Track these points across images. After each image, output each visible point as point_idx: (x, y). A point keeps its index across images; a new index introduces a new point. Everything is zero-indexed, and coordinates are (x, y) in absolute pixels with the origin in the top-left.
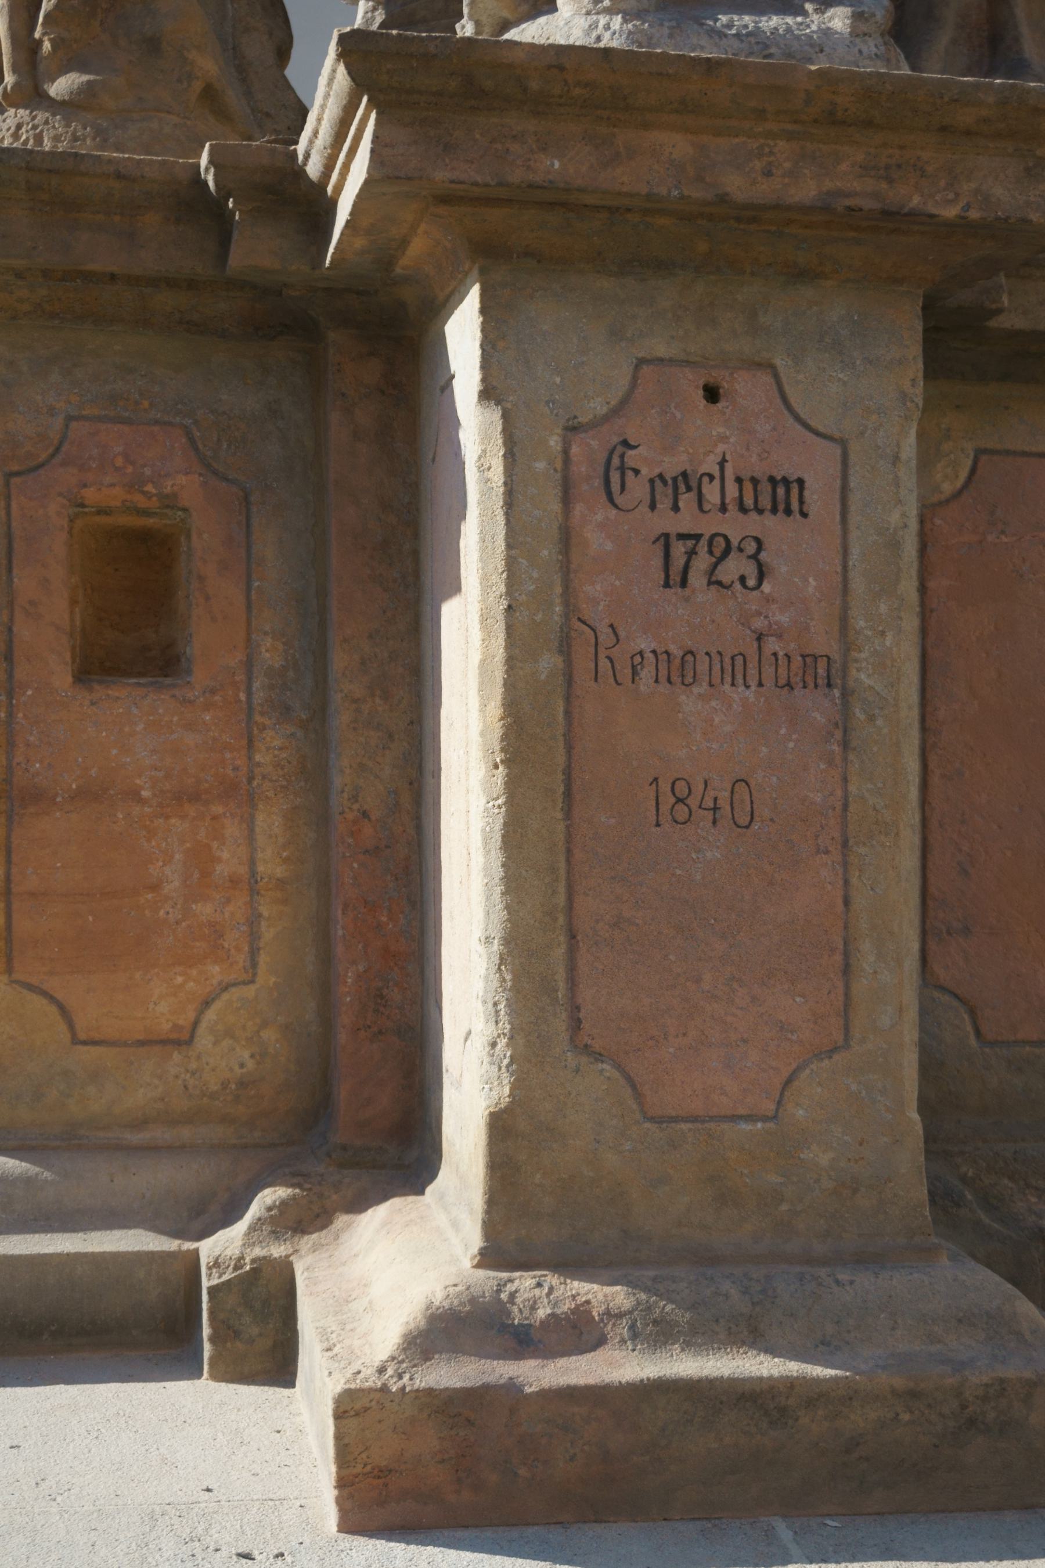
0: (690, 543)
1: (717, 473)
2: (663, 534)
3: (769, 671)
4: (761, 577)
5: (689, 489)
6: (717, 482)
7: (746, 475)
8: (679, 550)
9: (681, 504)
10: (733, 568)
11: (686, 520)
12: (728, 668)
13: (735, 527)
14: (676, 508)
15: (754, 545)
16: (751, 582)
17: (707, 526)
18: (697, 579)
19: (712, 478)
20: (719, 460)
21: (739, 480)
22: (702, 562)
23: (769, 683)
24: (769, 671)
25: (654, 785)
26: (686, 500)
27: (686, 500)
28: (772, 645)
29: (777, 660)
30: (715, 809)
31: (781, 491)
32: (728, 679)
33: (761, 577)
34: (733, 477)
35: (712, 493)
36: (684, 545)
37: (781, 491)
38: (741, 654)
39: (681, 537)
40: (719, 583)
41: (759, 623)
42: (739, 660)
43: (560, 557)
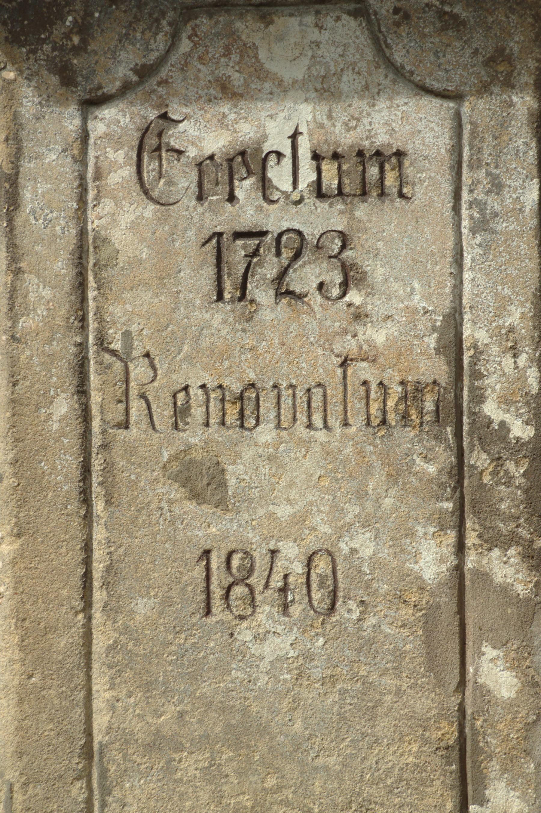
0: (253, 242)
1: (287, 151)
2: (215, 234)
3: (356, 405)
4: (345, 286)
5: (250, 173)
6: (287, 162)
7: (325, 150)
8: (238, 252)
9: (239, 193)
10: (308, 276)
11: (248, 209)
12: (302, 405)
13: (317, 220)
14: (232, 198)
15: (338, 243)
16: (336, 292)
17: (276, 219)
18: (262, 294)
19: (279, 155)
20: (291, 133)
21: (316, 157)
22: (269, 269)
23: (357, 421)
24: (356, 405)
25: (239, 405)
26: (245, 188)
27: (245, 188)
28: (363, 371)
29: (368, 391)
30: (284, 590)
31: (373, 171)
32: (302, 418)
33: (345, 286)
34: (309, 155)
35: (279, 175)
36: (244, 247)
37: (373, 171)
38: (319, 385)
39: (238, 235)
40: (289, 293)
41: (348, 345)
42: (317, 393)
43: (471, 10)
